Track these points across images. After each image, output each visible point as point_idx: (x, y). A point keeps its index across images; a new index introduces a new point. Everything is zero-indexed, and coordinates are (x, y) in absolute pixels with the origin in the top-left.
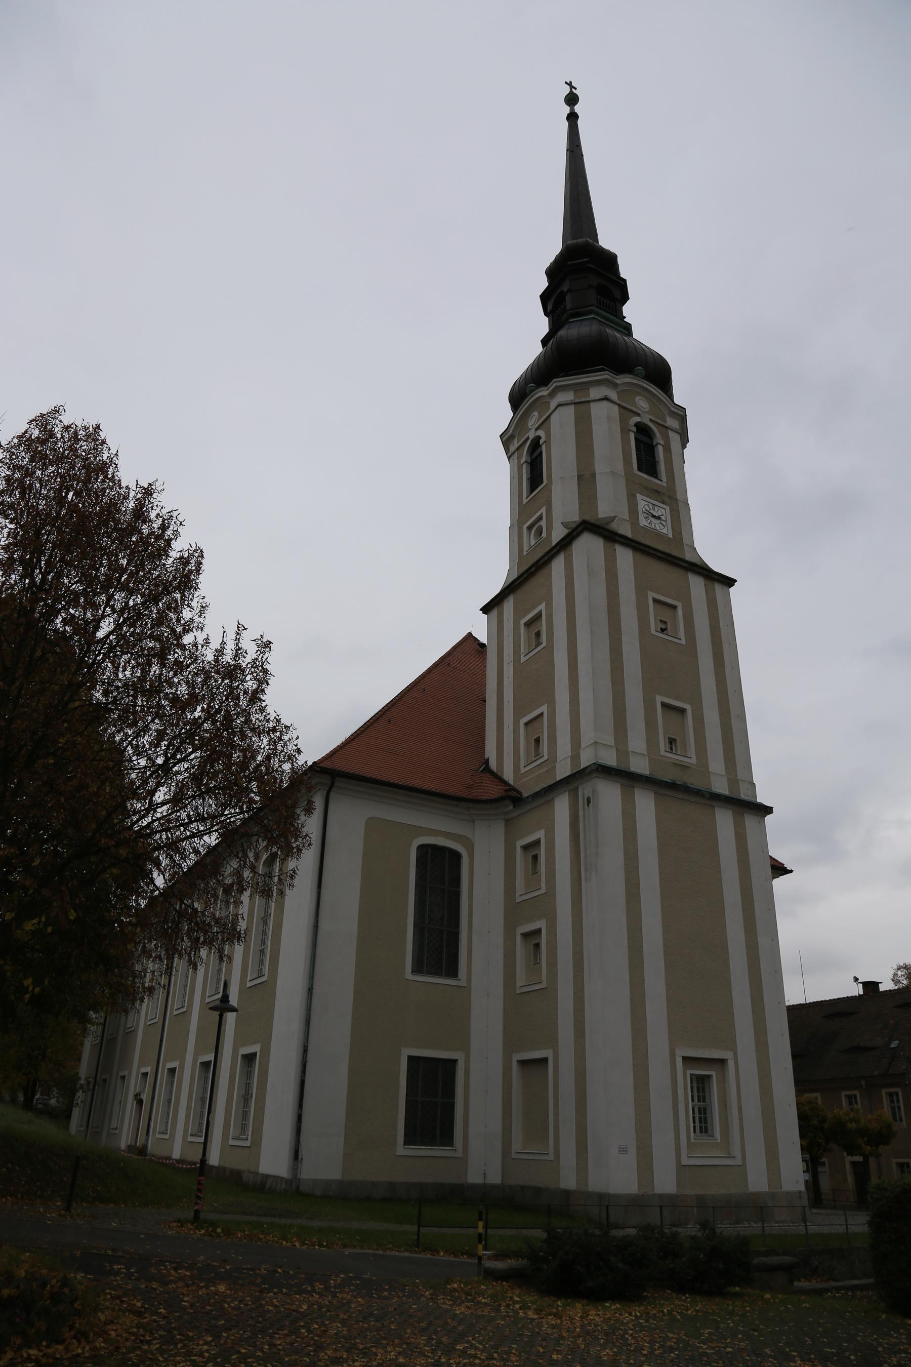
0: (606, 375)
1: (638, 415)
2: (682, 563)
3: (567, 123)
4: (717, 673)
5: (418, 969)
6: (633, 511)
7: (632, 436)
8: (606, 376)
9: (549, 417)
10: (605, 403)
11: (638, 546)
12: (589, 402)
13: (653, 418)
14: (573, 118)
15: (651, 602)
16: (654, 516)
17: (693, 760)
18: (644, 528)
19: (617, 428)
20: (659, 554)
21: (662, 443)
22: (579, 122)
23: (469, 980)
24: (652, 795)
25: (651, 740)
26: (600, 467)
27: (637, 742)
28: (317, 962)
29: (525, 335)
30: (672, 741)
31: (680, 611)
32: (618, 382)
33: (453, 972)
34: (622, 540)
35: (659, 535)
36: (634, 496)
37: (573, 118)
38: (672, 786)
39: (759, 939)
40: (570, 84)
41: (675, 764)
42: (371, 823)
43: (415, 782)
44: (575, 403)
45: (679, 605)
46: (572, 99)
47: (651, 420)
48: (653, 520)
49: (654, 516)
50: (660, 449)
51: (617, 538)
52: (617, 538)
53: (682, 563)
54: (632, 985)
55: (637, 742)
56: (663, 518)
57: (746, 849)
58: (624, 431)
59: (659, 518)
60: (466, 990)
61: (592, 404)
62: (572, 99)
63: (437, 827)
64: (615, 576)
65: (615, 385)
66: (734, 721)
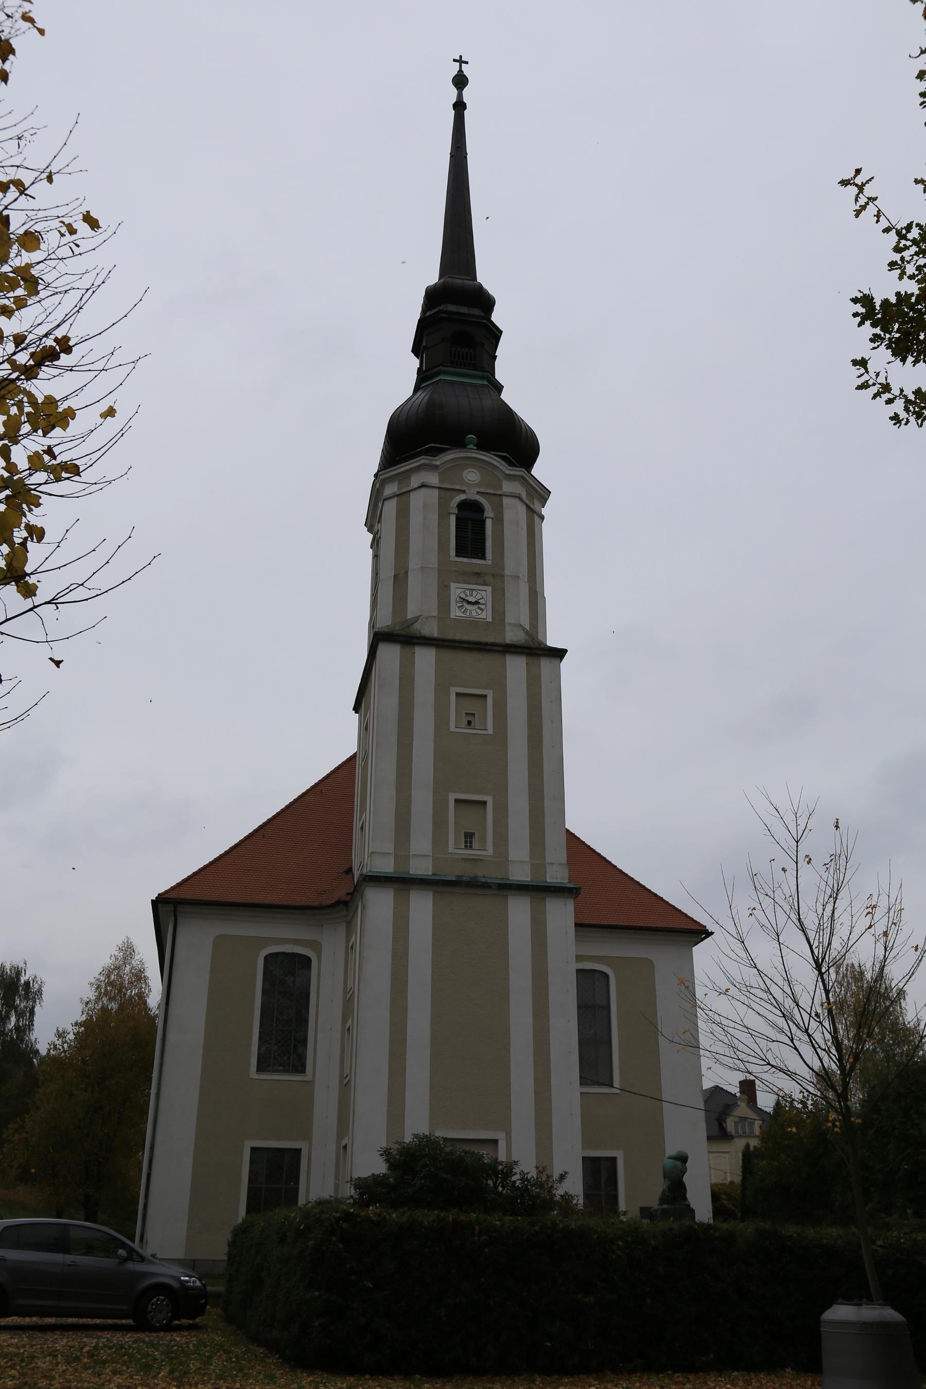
1: (464, 492)
2: (495, 648)
4: (530, 756)
5: (262, 1067)
6: (444, 604)
7: (453, 519)
8: (423, 461)
9: (409, 491)
10: (423, 490)
11: (440, 643)
12: (409, 491)
13: (482, 490)
14: (460, 106)
15: (453, 698)
16: (469, 603)
17: (490, 851)
18: (457, 621)
19: (434, 517)
20: (466, 645)
21: (491, 515)
24: (431, 894)
26: (414, 564)
27: (421, 843)
29: (395, 378)
30: (469, 836)
31: (490, 700)
32: (438, 463)
33: (300, 1067)
34: (421, 641)
35: (474, 624)
36: (448, 587)
37: (460, 106)
38: (457, 883)
39: (551, 1021)
40: (460, 61)
41: (465, 860)
42: (219, 941)
43: (260, 899)
44: (398, 495)
45: (490, 694)
46: (460, 81)
47: (478, 493)
48: (470, 607)
49: (469, 603)
50: (489, 524)
51: (415, 641)
52: (415, 641)
53: (495, 648)
54: (391, 1074)
55: (421, 843)
56: (482, 601)
57: (545, 935)
58: (443, 517)
59: (477, 603)
60: (311, 1083)
61: (411, 494)
62: (460, 81)
63: (285, 936)
64: (412, 681)
65: (436, 467)
66: (548, 803)
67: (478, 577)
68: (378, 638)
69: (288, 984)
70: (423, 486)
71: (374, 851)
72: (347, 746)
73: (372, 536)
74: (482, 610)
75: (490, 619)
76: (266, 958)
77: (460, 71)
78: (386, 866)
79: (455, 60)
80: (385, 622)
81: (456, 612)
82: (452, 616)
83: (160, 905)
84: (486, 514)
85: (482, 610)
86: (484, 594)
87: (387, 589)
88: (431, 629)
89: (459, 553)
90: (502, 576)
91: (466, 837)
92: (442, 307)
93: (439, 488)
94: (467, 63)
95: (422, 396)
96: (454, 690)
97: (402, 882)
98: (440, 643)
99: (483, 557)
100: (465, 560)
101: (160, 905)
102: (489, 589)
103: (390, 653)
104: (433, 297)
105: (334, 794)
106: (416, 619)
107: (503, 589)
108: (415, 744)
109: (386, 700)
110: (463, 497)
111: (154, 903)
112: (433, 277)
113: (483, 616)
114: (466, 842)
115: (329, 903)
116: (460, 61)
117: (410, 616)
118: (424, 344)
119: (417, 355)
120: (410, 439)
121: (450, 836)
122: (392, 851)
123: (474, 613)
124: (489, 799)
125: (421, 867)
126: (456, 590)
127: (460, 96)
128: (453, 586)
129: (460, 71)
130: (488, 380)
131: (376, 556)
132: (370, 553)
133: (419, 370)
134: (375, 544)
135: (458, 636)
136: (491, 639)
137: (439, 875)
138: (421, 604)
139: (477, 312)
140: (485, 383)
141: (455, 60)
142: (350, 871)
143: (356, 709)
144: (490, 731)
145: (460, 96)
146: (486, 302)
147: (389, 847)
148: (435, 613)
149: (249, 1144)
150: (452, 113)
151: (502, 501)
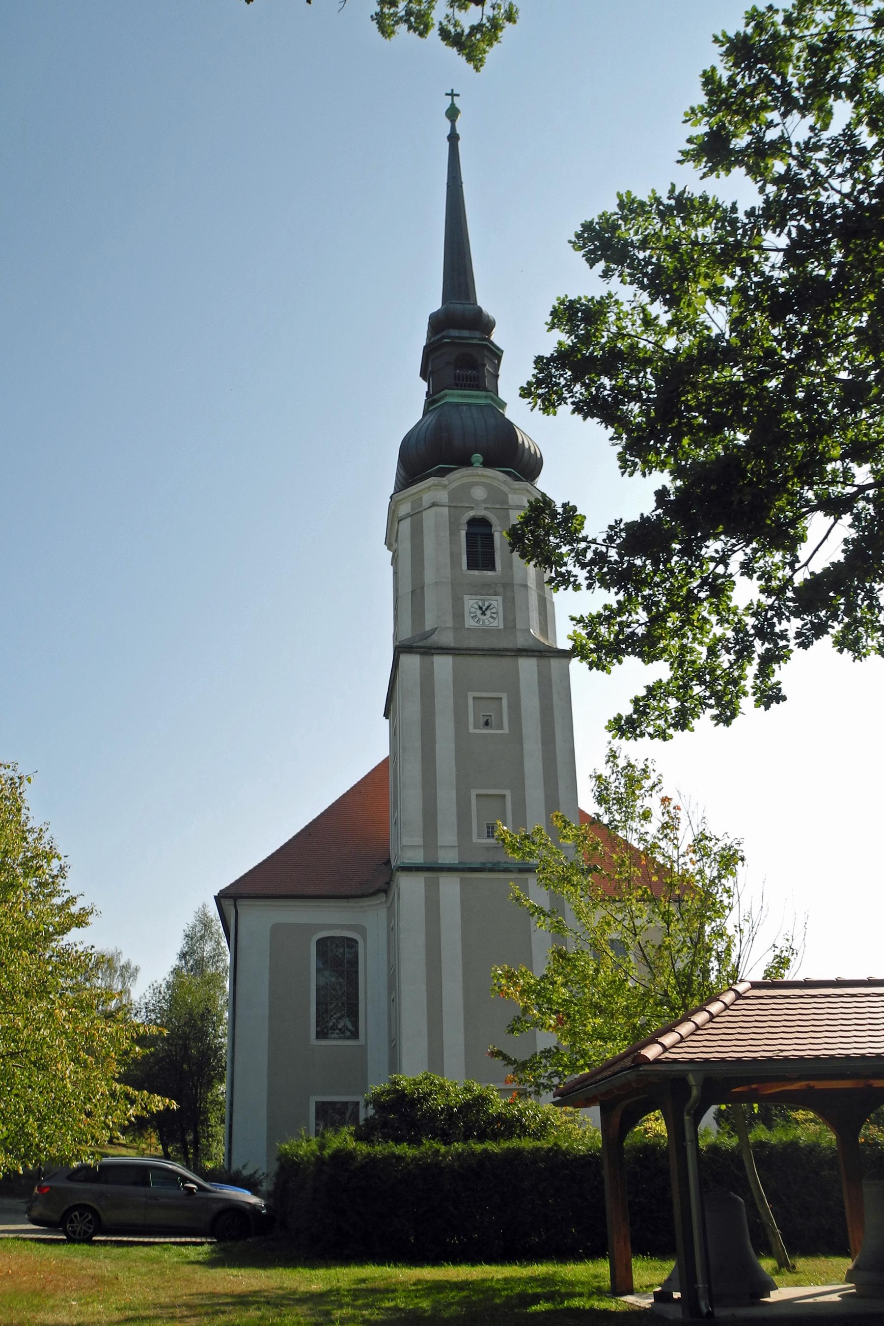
0: (432, 481)
3: (448, 144)
6: (458, 615)
7: (463, 533)
9: (422, 511)
10: (434, 509)
14: (453, 138)
15: (470, 702)
19: (445, 534)
22: (459, 143)
23: (366, 1040)
25: (463, 830)
26: (429, 576)
27: (447, 836)
28: (237, 1041)
29: (407, 402)
31: (505, 702)
32: (446, 482)
35: (486, 632)
37: (453, 138)
40: (452, 95)
46: (452, 113)
51: (433, 651)
52: (433, 651)
55: (447, 836)
58: (454, 532)
60: (364, 1047)
61: (424, 513)
62: (452, 113)
65: (445, 486)
67: (487, 589)
68: (400, 650)
69: (339, 959)
70: (434, 505)
71: (408, 847)
72: (381, 751)
73: (391, 553)
74: (494, 618)
75: (501, 627)
76: (318, 942)
77: (453, 104)
78: (417, 857)
79: (447, 94)
80: (407, 634)
81: (470, 623)
82: (467, 626)
83: (222, 900)
84: (493, 529)
85: (494, 618)
86: (497, 602)
87: (406, 603)
88: (447, 639)
89: (471, 566)
90: (512, 585)
91: (488, 828)
92: (444, 333)
93: (449, 506)
94: (458, 95)
95: (431, 418)
96: (471, 695)
97: (432, 868)
98: (456, 652)
99: (492, 568)
100: (476, 572)
101: (222, 900)
102: (500, 598)
103: (411, 661)
104: (437, 324)
105: (374, 787)
106: (433, 631)
107: (513, 598)
108: (438, 746)
109: (411, 709)
110: (472, 513)
111: (217, 898)
112: (436, 304)
113: (495, 624)
114: (488, 832)
115: (371, 891)
116: (452, 95)
117: (428, 628)
118: (430, 369)
119: (424, 379)
120: (424, 458)
121: (457, 935)
122: (421, 843)
123: (487, 622)
124: (508, 793)
125: (448, 857)
126: (470, 603)
127: (453, 128)
128: (466, 597)
129: (453, 104)
130: (493, 399)
131: (395, 573)
132: (390, 569)
133: (427, 393)
134: (395, 561)
135: (473, 644)
136: (505, 644)
137: (465, 864)
138: (436, 616)
139: (477, 334)
140: (489, 402)
141: (447, 94)
142: (388, 862)
143: (386, 715)
144: (506, 731)
145: (453, 128)
146: (485, 325)
147: (419, 841)
148: (450, 624)
149: (313, 1100)
150: (446, 145)
151: (508, 515)
